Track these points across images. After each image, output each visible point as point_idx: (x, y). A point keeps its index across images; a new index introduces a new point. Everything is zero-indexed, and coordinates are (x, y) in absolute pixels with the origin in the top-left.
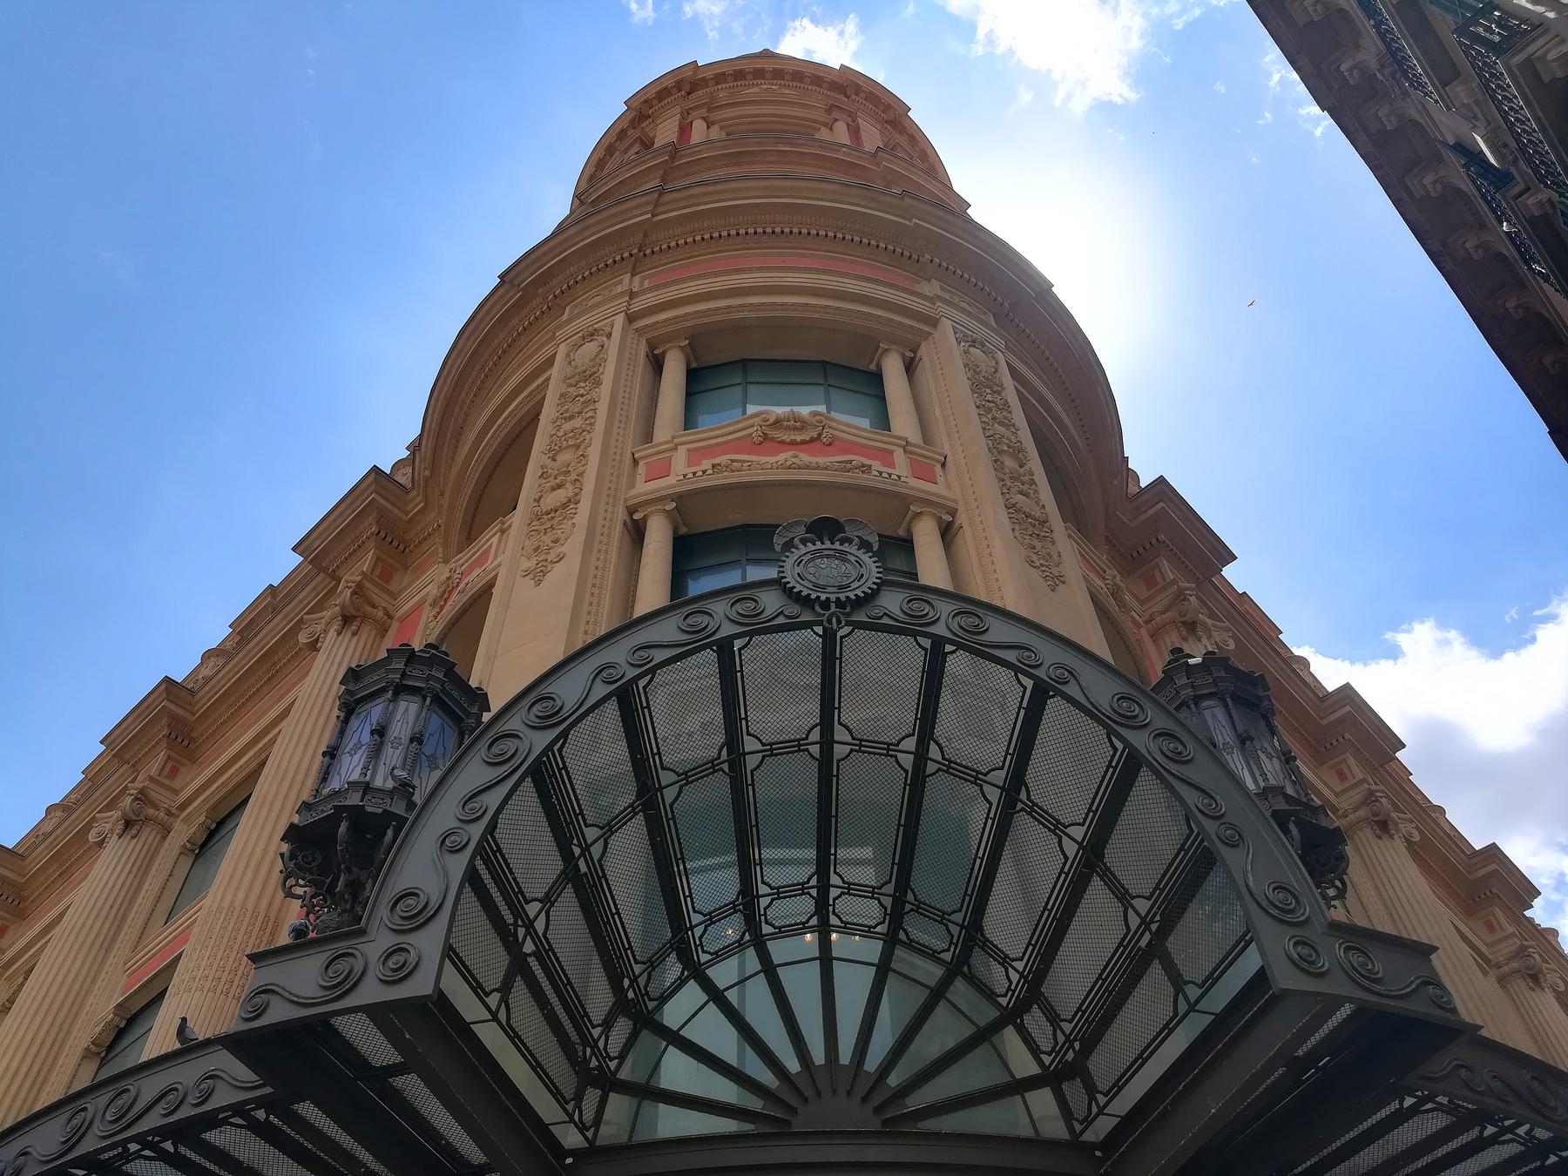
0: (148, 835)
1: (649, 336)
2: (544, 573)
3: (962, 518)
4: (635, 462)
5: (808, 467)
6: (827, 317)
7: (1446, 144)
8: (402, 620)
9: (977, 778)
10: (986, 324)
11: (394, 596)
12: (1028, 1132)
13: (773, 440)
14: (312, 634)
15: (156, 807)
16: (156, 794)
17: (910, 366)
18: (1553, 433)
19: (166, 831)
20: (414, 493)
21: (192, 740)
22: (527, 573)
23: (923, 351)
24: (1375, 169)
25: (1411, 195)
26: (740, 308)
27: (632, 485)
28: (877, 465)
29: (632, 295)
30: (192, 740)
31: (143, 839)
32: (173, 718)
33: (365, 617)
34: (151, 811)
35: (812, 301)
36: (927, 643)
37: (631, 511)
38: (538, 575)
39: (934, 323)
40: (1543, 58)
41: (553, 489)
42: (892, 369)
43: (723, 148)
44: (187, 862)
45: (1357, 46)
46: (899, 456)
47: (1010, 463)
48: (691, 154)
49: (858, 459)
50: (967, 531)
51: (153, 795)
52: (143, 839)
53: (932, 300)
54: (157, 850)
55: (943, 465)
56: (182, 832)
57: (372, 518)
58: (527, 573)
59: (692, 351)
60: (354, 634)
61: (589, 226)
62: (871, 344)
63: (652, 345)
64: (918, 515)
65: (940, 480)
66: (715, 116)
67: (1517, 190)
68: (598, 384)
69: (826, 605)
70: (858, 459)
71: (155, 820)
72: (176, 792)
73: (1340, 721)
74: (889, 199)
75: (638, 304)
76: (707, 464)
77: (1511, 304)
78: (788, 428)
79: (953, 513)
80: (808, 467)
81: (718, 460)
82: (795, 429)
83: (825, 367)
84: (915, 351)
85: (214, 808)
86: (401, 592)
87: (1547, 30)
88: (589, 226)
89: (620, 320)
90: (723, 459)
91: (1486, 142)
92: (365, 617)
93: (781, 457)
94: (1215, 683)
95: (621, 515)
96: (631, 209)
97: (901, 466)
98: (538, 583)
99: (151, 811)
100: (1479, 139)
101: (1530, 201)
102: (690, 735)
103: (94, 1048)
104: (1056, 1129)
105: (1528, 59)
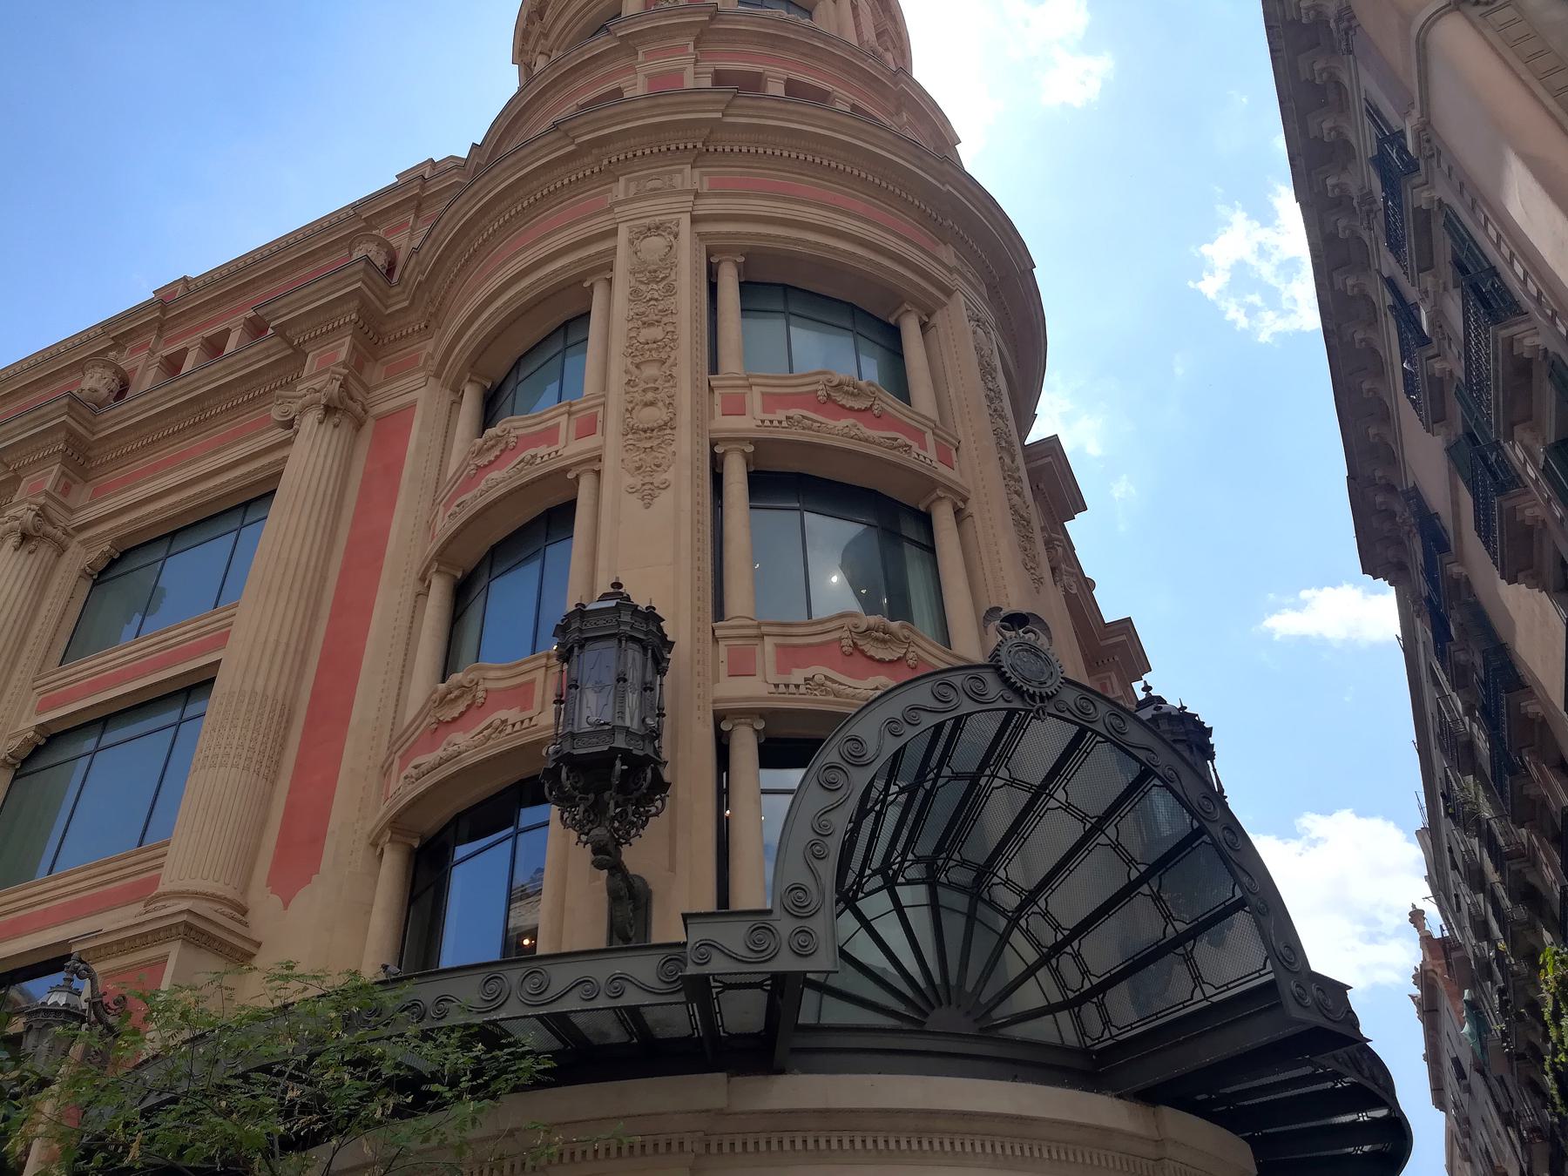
0: (45, 552)
1: (709, 243)
2: (653, 497)
3: (972, 507)
5: (866, 440)
6: (868, 269)
7: (1379, 272)
9: (1116, 846)
10: (980, 294)
12: (1057, 1041)
13: (834, 402)
14: (286, 414)
15: (53, 524)
16: (55, 512)
17: (924, 327)
18: (1351, 479)
19: (61, 550)
20: (398, 289)
21: (88, 459)
22: (632, 490)
23: (938, 319)
24: (1312, 250)
25: (1332, 285)
26: (798, 241)
29: (697, 195)
30: (88, 459)
31: (40, 556)
32: (71, 433)
33: (346, 410)
34: (49, 529)
35: (860, 251)
36: (1196, 824)
37: (713, 444)
38: (648, 496)
39: (948, 292)
40: (1520, 341)
41: (646, 405)
42: (911, 329)
43: (760, 25)
44: (88, 585)
45: (1344, 168)
46: (929, 437)
48: (728, 22)
49: (903, 439)
51: (51, 512)
52: (40, 556)
53: (950, 270)
54: (53, 568)
56: (79, 557)
57: (355, 304)
58: (632, 490)
59: (742, 269)
60: (336, 426)
61: (658, 106)
62: (896, 297)
64: (940, 498)
65: (956, 465)
67: (1431, 353)
68: (670, 290)
69: (1032, 697)
70: (903, 439)
71: (53, 539)
72: (72, 511)
73: (1117, 645)
74: (931, 160)
75: (708, 206)
76: (780, 415)
77: (1366, 386)
78: (847, 393)
79: (965, 500)
80: (866, 440)
81: (791, 413)
82: (852, 394)
83: (854, 310)
84: (929, 316)
85: (119, 539)
86: (377, 387)
87: (1529, 320)
88: (658, 106)
90: (795, 412)
91: (1428, 318)
92: (346, 410)
93: (842, 423)
94: (1187, 733)
96: (704, 102)
97: (931, 454)
98: (648, 506)
99: (49, 529)
100: (1423, 313)
101: (1437, 366)
102: (797, 686)
103: (10, 760)
104: (1071, 1038)
105: (1511, 337)
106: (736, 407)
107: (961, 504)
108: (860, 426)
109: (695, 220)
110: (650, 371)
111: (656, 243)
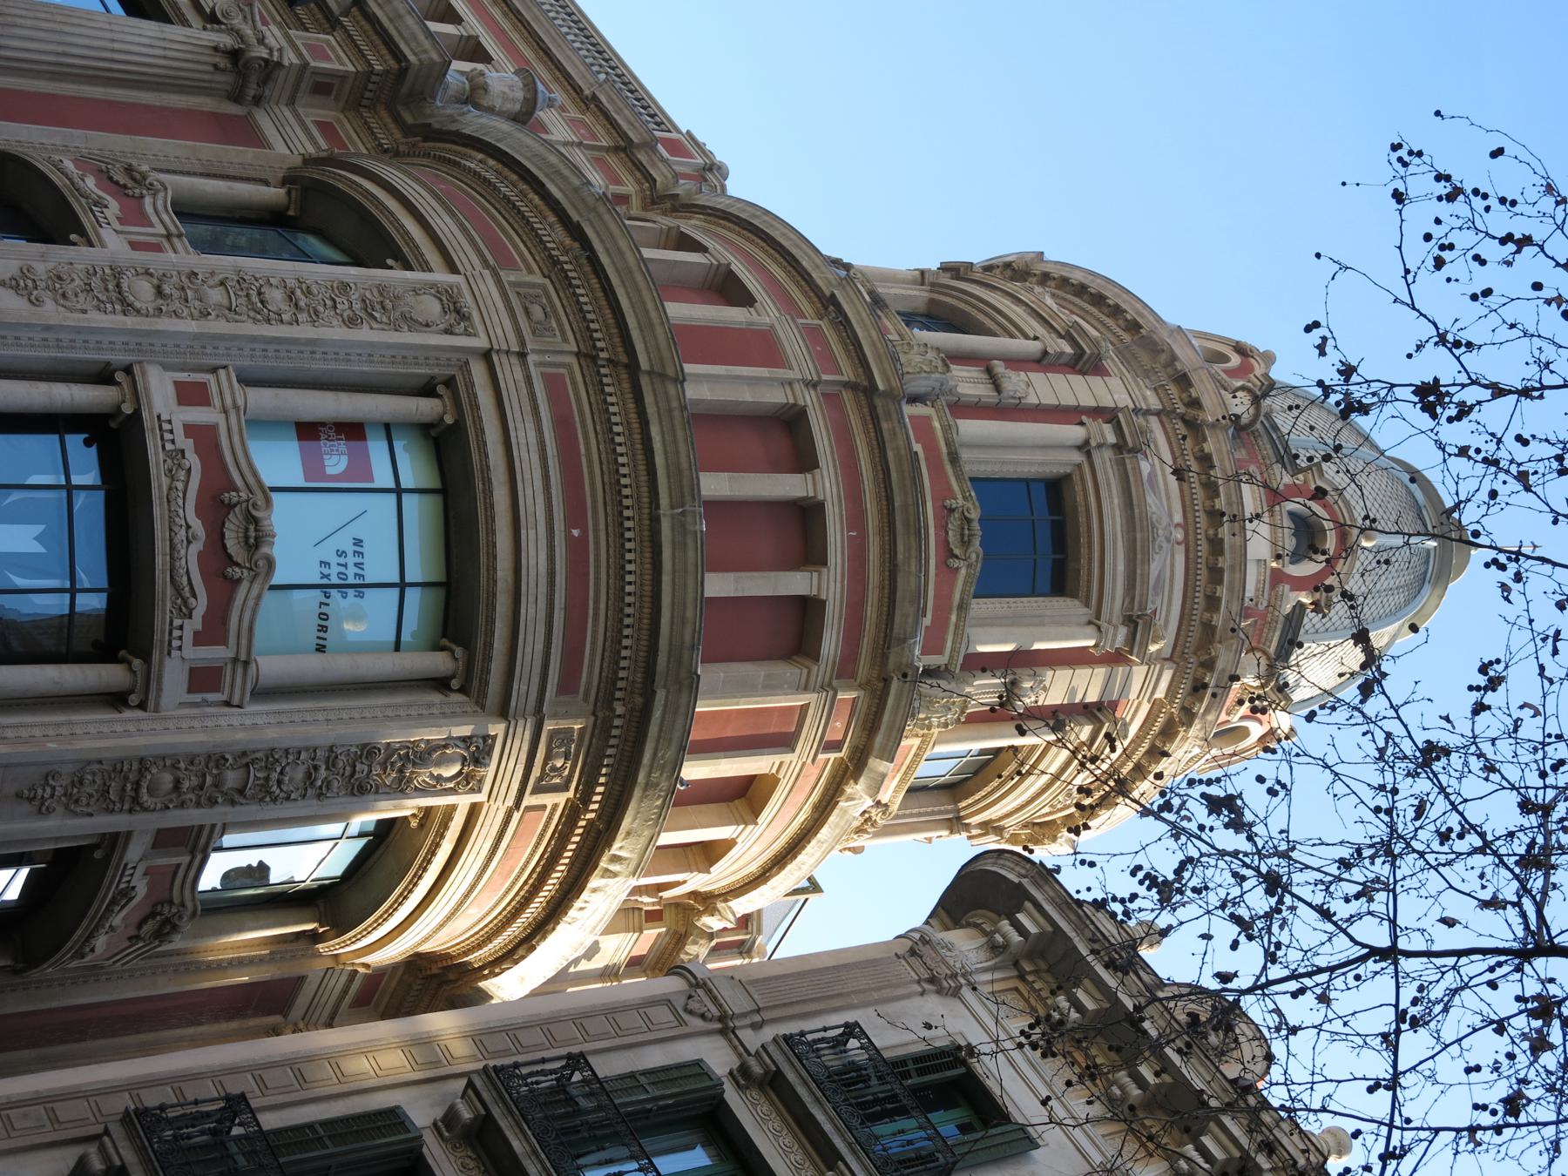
4: (214, 370)
8: (247, 120)
11: (291, 102)
17: (440, 684)
22: (26, 272)
23: (457, 698)
27: (166, 367)
28: (196, 622)
39: (503, 713)
47: (232, 778)
50: (117, 716)
55: (228, 704)
58: (26, 272)
63: (450, 382)
66: (1104, 461)
68: (352, 322)
75: (510, 373)
76: (188, 445)
79: (142, 706)
89: (481, 342)
90: (193, 460)
93: (197, 526)
95: (120, 358)
106: (190, 394)
107: (134, 699)
108: (197, 547)
109: (487, 356)
110: (232, 778)
111: (430, 307)
